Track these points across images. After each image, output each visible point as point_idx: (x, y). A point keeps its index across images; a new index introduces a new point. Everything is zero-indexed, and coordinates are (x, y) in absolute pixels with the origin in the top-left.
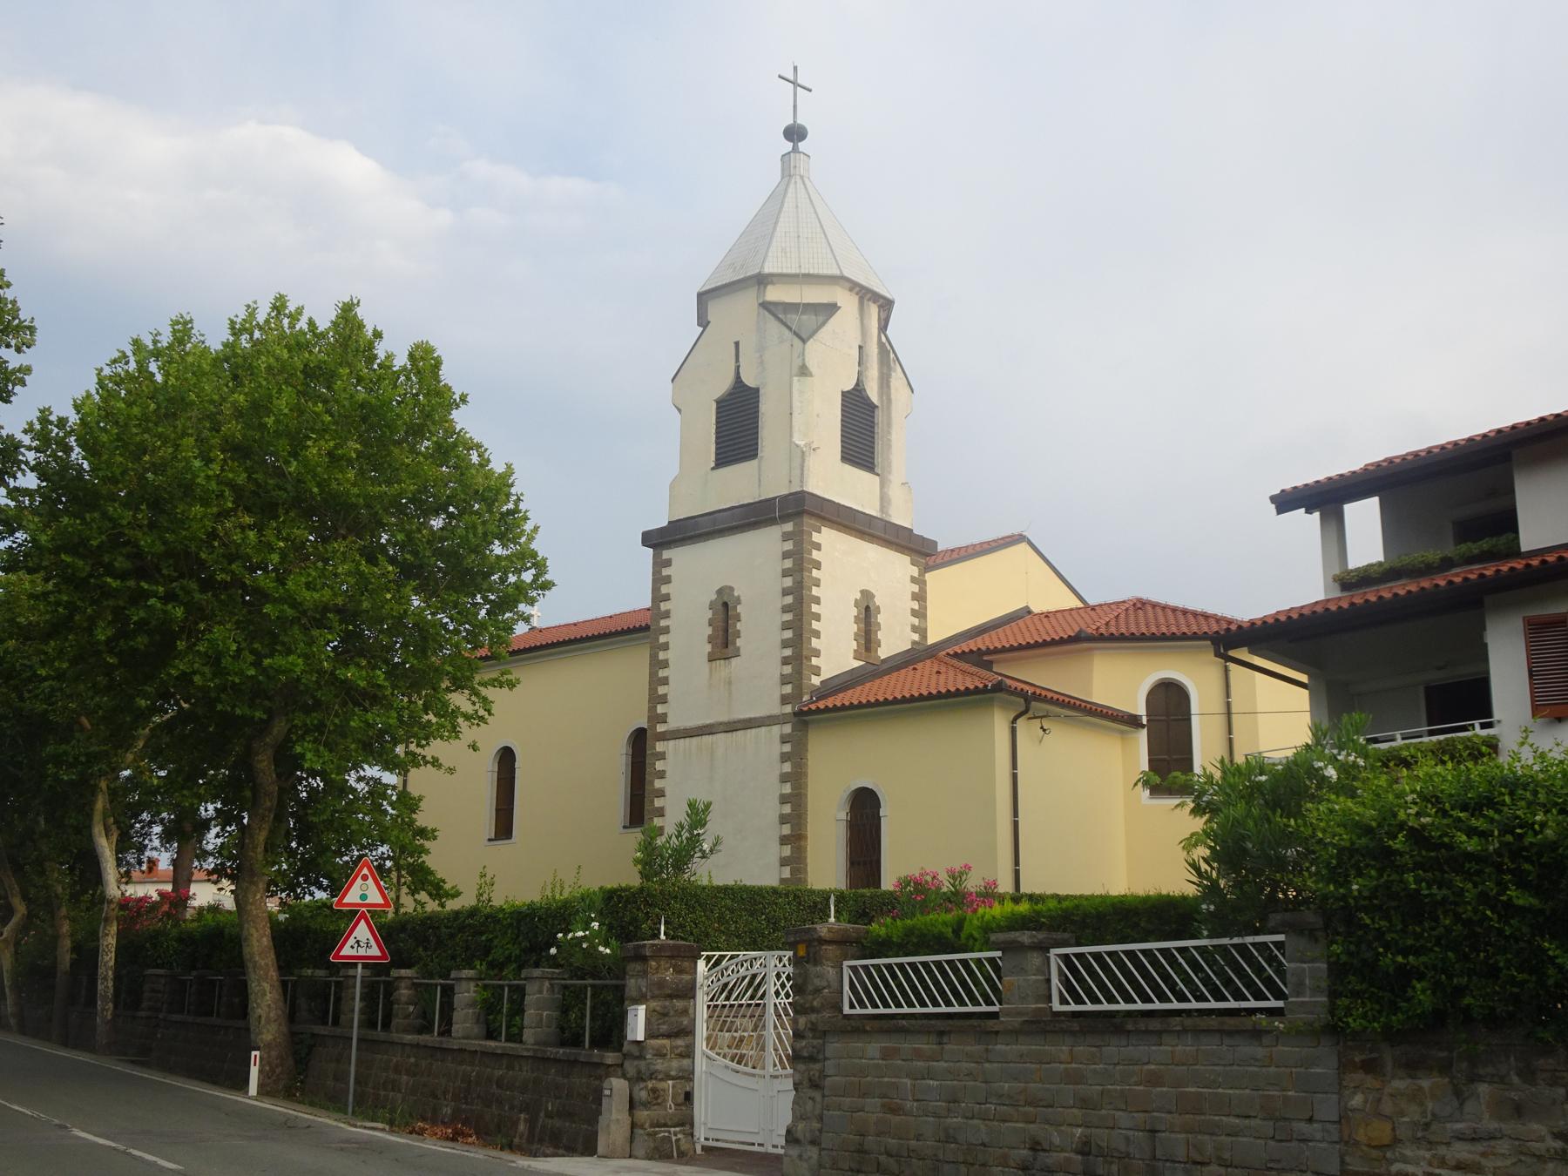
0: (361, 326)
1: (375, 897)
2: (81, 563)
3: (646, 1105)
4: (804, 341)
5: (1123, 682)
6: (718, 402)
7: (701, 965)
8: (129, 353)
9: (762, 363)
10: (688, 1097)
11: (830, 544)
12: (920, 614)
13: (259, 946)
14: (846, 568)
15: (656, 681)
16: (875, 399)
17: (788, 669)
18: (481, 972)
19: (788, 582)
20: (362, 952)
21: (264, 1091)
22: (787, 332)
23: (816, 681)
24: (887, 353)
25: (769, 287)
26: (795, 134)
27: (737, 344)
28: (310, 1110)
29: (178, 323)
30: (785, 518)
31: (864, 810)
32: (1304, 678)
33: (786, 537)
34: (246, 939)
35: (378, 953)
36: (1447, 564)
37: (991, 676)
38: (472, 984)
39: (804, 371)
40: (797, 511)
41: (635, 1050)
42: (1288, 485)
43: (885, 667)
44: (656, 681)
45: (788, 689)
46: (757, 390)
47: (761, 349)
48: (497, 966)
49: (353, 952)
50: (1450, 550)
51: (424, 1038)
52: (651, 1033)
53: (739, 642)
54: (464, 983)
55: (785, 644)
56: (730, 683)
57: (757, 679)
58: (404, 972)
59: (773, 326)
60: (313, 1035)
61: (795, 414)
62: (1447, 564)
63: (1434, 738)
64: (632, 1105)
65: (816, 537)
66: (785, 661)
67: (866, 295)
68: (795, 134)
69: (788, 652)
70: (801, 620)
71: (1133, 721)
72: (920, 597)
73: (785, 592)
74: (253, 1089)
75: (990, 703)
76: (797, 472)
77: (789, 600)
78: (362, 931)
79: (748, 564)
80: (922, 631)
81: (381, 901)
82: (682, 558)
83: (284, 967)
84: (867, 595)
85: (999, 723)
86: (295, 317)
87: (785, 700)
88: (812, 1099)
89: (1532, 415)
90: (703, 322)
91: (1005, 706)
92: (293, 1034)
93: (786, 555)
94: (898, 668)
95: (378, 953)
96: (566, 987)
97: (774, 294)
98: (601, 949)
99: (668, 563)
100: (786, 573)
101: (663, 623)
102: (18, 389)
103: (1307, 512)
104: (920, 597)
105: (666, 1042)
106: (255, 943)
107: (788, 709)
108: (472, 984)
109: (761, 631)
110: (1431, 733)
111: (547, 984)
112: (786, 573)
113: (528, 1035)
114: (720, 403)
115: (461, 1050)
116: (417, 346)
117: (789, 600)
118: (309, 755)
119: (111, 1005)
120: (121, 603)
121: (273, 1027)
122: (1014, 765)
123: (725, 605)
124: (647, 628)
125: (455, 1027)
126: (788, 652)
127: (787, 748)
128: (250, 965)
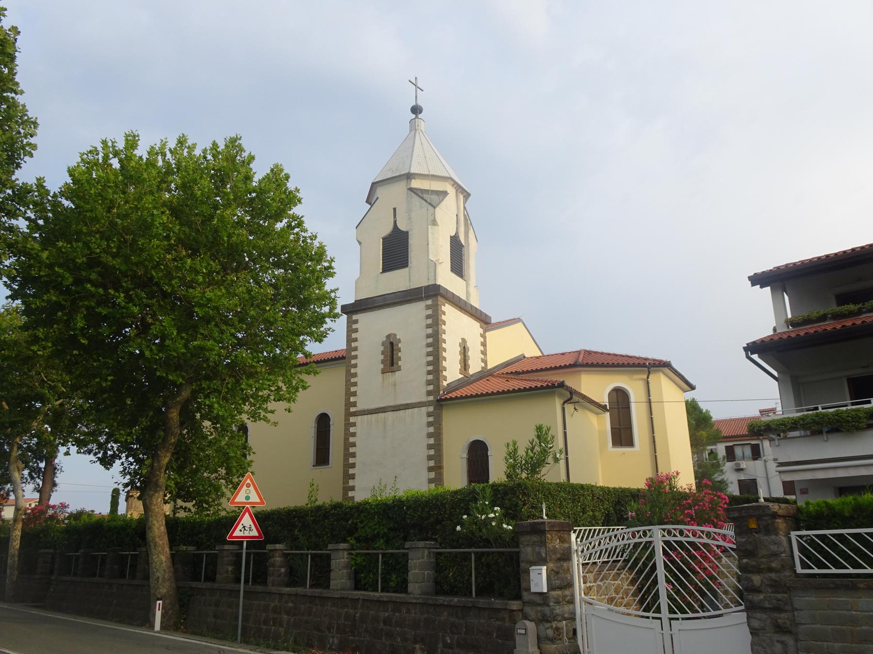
0: (242, 150)
1: (254, 498)
2: (67, 275)
3: (552, 640)
4: (435, 208)
5: (597, 386)
6: (384, 239)
7: (573, 536)
8: (100, 149)
9: (410, 218)
10: (575, 632)
11: (450, 314)
12: (484, 353)
13: (158, 530)
14: (456, 326)
15: (349, 384)
16: (463, 242)
17: (430, 377)
18: (352, 545)
19: (430, 331)
20: (247, 534)
21: (163, 627)
22: (424, 203)
23: (445, 383)
24: (467, 218)
25: (413, 180)
26: (416, 110)
27: (395, 209)
28: (215, 641)
29: (129, 135)
30: (427, 297)
31: (478, 454)
32: (775, 373)
33: (428, 307)
34: (150, 528)
35: (257, 534)
36: (823, 318)
37: (542, 382)
38: (346, 553)
39: (434, 223)
40: (433, 294)
41: (538, 600)
42: (759, 270)
43: (472, 379)
44: (349, 384)
45: (431, 388)
46: (407, 233)
47: (409, 211)
48: (368, 541)
49: (241, 534)
50: (835, 308)
51: (299, 590)
52: (551, 587)
53: (400, 363)
54: (341, 553)
55: (429, 364)
56: (395, 385)
57: (411, 382)
58: (278, 546)
59: (416, 200)
60: (191, 588)
61: (430, 245)
62: (823, 318)
63: (854, 407)
64: (539, 639)
65: (443, 308)
66: (429, 373)
67: (459, 189)
68: (416, 110)
69: (430, 368)
70: (438, 351)
71: (603, 408)
72: (484, 344)
73: (428, 336)
74: (157, 627)
75: (552, 394)
76: (433, 274)
77: (430, 340)
78: (247, 520)
79: (407, 322)
80: (484, 361)
81: (259, 501)
82: (363, 319)
83: (172, 542)
84: (464, 340)
85: (558, 402)
86: (191, 148)
87: (429, 393)
88: (782, 642)
89: (847, 246)
90: (370, 200)
91: (561, 395)
92: (178, 588)
93: (428, 317)
94: (481, 378)
95: (257, 534)
96: (440, 554)
97: (415, 184)
98: (505, 526)
99: (356, 322)
100: (428, 326)
101: (353, 353)
102: (27, 158)
103: (761, 287)
104: (484, 344)
105: (559, 592)
106: (156, 530)
107: (431, 398)
108: (346, 553)
109: (413, 357)
110: (853, 404)
111: (426, 552)
112: (428, 326)
113: (414, 588)
114: (385, 239)
115: (342, 598)
116: (277, 166)
117: (430, 340)
118: (216, 406)
119: (16, 572)
120: (93, 304)
121: (167, 584)
122: (565, 428)
123: (392, 344)
124: (343, 358)
125: (332, 583)
126: (430, 368)
127: (431, 419)
128: (152, 544)
